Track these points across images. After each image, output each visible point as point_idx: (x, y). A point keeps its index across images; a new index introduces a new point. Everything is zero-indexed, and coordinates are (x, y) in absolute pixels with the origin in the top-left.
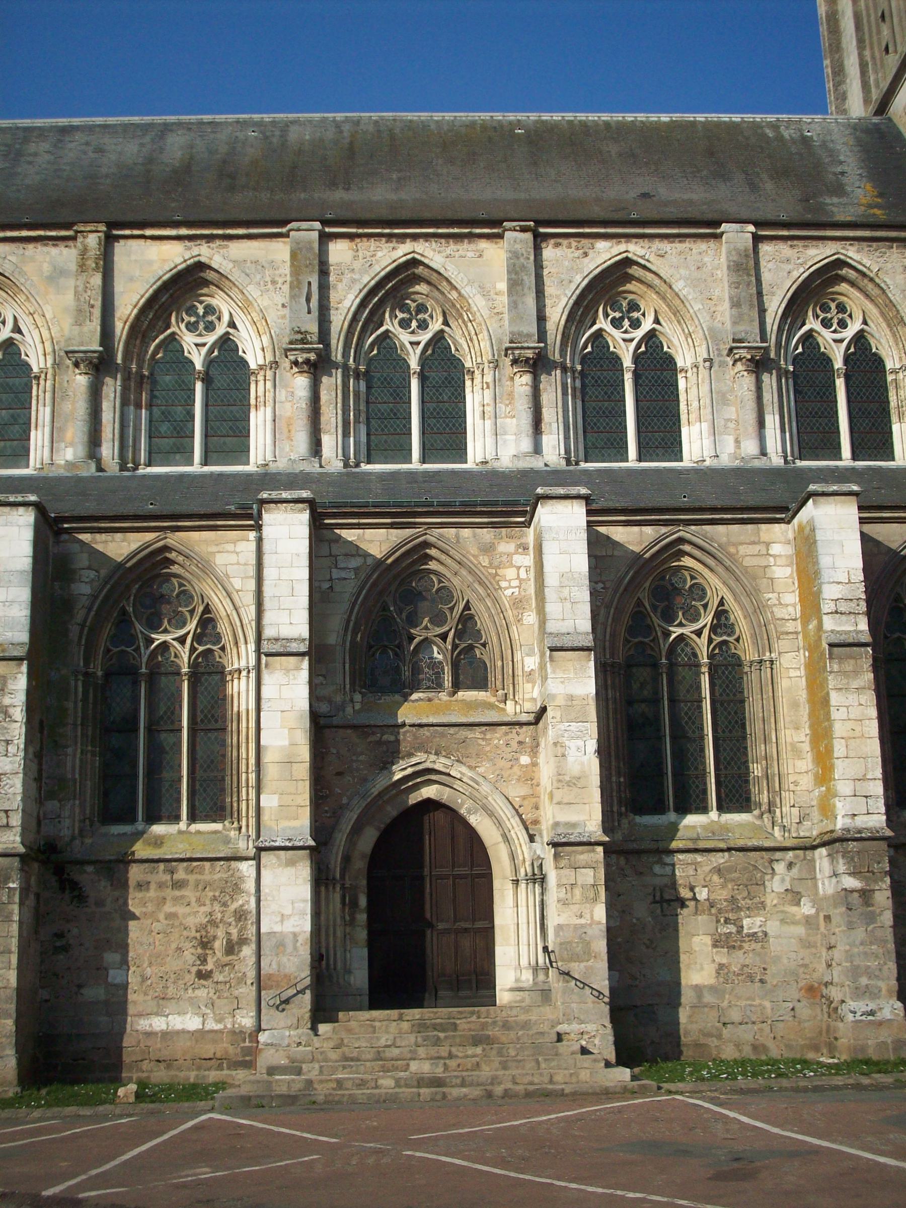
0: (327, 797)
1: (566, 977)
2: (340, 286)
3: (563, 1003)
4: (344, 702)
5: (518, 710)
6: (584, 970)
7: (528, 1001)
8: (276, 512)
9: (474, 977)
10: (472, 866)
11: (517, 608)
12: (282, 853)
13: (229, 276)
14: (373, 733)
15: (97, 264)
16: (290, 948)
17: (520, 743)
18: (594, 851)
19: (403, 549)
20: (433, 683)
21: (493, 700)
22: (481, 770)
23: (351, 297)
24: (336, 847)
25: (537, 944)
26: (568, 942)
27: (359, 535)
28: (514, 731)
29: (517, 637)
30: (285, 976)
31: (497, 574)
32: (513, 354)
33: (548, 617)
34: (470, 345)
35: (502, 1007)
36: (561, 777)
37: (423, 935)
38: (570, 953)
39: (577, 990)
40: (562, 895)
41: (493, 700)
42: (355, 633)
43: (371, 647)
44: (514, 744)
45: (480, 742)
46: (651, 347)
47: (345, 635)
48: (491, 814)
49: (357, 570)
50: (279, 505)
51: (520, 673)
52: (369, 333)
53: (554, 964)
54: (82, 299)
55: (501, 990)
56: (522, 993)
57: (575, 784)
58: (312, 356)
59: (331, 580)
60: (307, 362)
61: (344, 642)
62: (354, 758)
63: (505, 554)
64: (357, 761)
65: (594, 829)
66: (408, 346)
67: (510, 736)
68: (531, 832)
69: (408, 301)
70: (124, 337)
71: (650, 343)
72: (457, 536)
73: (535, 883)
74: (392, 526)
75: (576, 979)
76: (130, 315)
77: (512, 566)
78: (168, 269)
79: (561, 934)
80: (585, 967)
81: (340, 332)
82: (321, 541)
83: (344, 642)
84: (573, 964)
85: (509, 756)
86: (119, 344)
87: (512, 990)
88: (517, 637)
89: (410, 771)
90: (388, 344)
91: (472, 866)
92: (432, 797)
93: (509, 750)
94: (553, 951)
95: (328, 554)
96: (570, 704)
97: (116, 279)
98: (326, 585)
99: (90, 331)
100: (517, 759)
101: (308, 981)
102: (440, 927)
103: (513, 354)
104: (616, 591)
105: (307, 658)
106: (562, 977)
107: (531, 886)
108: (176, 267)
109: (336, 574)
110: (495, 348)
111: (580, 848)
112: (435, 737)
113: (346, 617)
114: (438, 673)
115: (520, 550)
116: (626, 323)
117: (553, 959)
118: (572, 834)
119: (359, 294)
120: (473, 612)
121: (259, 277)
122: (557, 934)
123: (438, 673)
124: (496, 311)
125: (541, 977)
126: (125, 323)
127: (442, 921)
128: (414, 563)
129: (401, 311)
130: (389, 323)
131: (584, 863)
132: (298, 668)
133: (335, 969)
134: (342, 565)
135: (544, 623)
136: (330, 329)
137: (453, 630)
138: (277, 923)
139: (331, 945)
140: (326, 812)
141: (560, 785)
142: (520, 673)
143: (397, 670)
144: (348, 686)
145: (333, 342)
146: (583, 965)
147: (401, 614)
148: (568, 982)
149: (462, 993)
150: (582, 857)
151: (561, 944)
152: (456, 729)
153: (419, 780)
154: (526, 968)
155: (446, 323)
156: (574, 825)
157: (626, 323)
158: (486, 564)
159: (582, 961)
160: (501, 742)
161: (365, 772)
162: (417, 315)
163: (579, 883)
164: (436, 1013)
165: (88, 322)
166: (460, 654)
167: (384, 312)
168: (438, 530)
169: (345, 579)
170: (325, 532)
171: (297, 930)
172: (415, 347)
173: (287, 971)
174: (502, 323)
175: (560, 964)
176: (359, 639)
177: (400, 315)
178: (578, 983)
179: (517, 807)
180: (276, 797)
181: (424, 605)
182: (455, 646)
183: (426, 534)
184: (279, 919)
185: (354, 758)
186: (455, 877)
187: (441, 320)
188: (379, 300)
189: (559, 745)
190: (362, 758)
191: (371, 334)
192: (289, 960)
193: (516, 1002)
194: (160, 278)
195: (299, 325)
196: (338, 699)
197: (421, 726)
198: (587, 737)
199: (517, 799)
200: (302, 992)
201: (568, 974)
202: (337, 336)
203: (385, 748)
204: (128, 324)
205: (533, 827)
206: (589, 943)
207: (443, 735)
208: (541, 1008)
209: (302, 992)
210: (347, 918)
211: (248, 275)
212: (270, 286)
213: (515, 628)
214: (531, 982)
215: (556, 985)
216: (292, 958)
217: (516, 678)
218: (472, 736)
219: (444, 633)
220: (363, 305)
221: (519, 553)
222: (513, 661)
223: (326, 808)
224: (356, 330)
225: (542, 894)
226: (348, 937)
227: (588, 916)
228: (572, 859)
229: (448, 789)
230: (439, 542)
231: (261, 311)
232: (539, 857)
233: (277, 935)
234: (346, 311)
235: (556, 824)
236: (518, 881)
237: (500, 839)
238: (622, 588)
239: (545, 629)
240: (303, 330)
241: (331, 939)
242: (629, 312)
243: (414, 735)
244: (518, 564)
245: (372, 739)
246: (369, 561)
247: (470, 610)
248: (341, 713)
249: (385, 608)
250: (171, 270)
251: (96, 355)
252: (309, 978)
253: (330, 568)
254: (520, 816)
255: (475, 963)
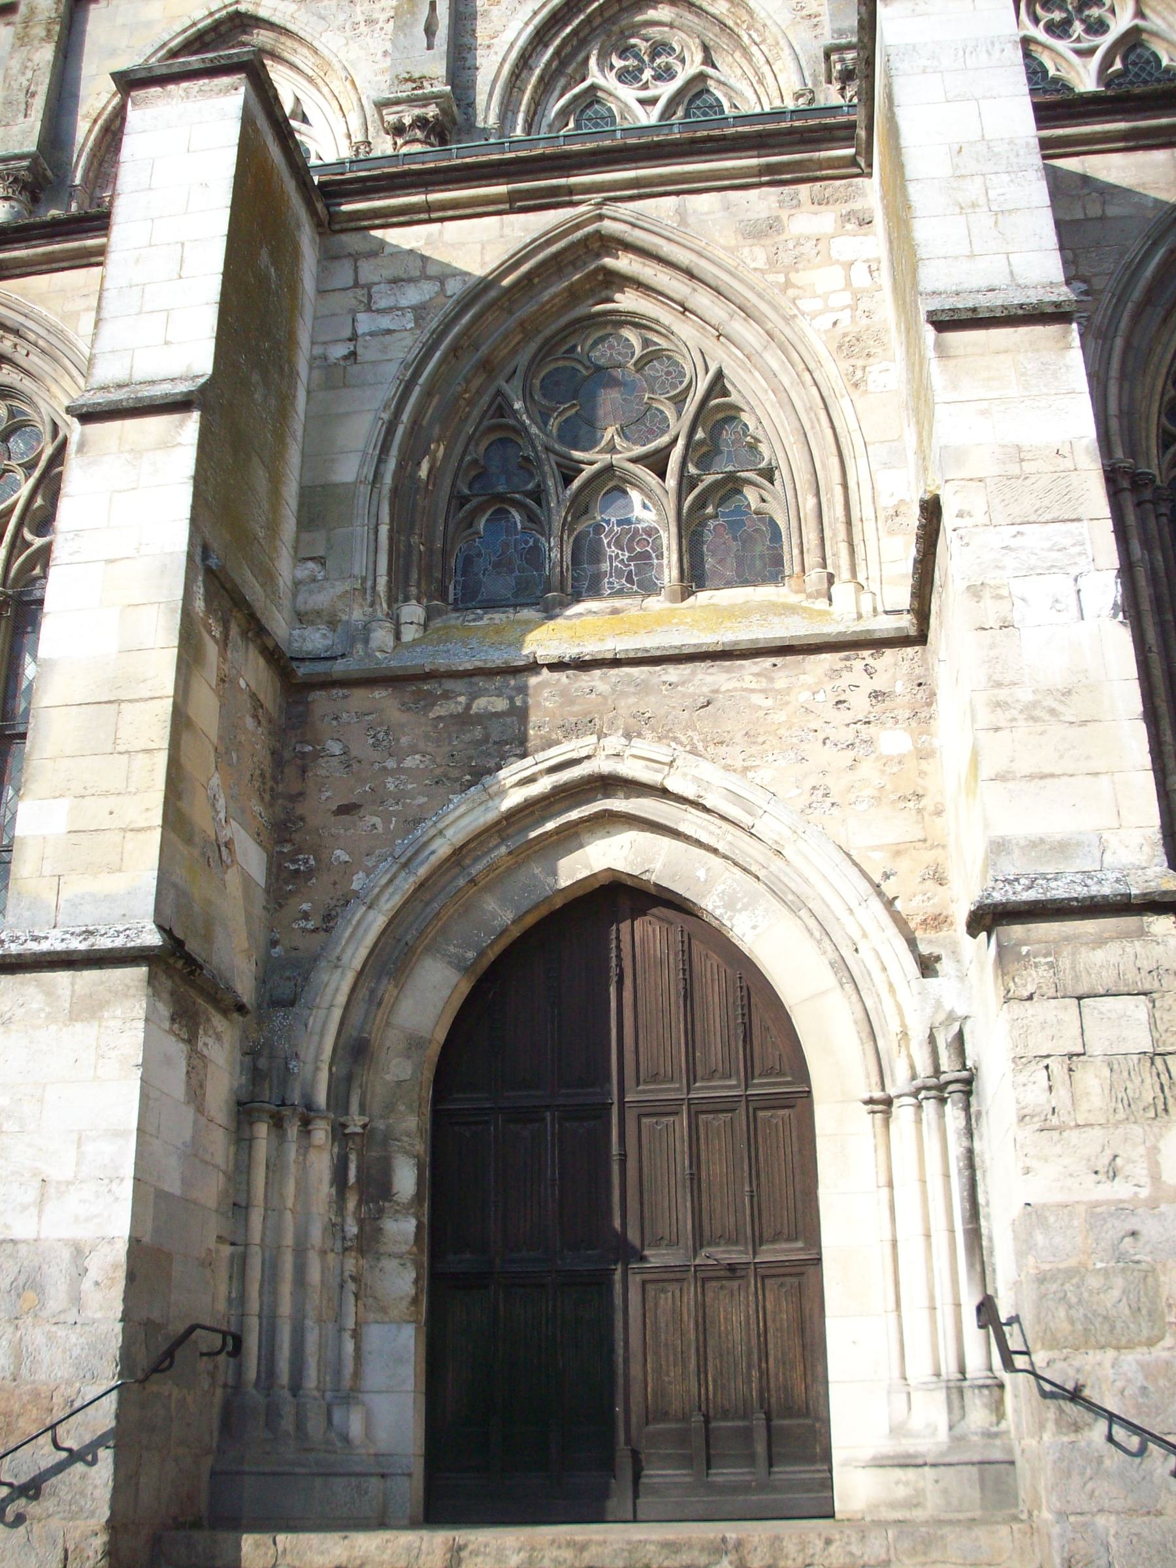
0: (310, 873)
1: (1068, 1407)
2: (495, 11)
3: (1062, 1515)
4: (373, 618)
5: (866, 609)
6: (1140, 1380)
7: (932, 1505)
8: (160, 102)
9: (758, 1421)
10: (749, 1076)
11: (848, 357)
12: (62, 978)
13: (290, 26)
14: (447, 696)
15: (49, 31)
16: (57, 1297)
17: (876, 695)
18: (1142, 933)
19: (541, 256)
20: (630, 580)
21: (794, 599)
22: (764, 775)
23: (516, 24)
24: (322, 1013)
25: (958, 1305)
26: (1070, 1273)
27: (429, 236)
28: (858, 665)
29: (853, 426)
30: (36, 1395)
31: (788, 284)
32: (842, 60)
33: (922, 252)
34: (760, 90)
35: (862, 1527)
36: (1002, 694)
37: (600, 1283)
38: (1078, 1313)
39: (1114, 1460)
40: (1036, 1096)
41: (794, 599)
42: (411, 459)
43: (463, 500)
44: (860, 703)
45: (757, 699)
46: (1134, 64)
47: (381, 460)
48: (795, 904)
49: (420, 312)
50: (171, 87)
51: (868, 513)
52: (557, 93)
53: (1020, 1361)
54: (15, 86)
55: (845, 1464)
56: (911, 1474)
57: (1052, 712)
58: (432, 111)
59: (354, 338)
60: (421, 122)
61: (378, 476)
62: (391, 764)
63: (808, 238)
64: (400, 770)
65: (1141, 858)
66: (637, 107)
67: (847, 679)
68: (924, 949)
69: (633, 41)
70: (90, 144)
71: (1132, 57)
72: (682, 215)
73: (942, 1101)
74: (515, 204)
75: (1112, 1418)
76: (104, 108)
77: (830, 261)
78: (179, 30)
79: (1040, 1238)
80: (1143, 1366)
81: (495, 81)
82: (336, 258)
83: (378, 476)
84: (1094, 1357)
85: (848, 735)
86: (79, 156)
87: (880, 1463)
88: (853, 426)
89: (544, 785)
90: (596, 112)
91: (749, 1076)
92: (621, 865)
93: (848, 716)
94: (1014, 1320)
95: (351, 283)
96: (1014, 469)
97: (86, 58)
98: (340, 351)
99: (23, 132)
100: (869, 742)
101: (104, 1416)
102: (654, 1262)
103: (842, 60)
104: (1121, 299)
105: (196, 415)
106: (1051, 1410)
107: (930, 1106)
108: (194, 24)
109: (365, 324)
110: (806, 74)
111: (1089, 926)
112: (623, 694)
113: (386, 416)
114: (646, 556)
115: (849, 226)
116: (1078, 28)
117: (1014, 1344)
118: (1057, 876)
119: (531, 19)
120: (734, 398)
121: (342, 17)
122: (1024, 1247)
123: (646, 556)
124: (805, 13)
125: (978, 1416)
126: (95, 121)
127: (657, 1243)
128: (574, 296)
129: (621, 56)
130: (598, 74)
131: (1107, 980)
132: (166, 445)
133: (296, 1387)
134: (382, 304)
135: (914, 271)
136: (474, 82)
137: (681, 442)
138: (24, 1208)
139: (285, 1307)
140: (306, 916)
141: (1001, 718)
142: (868, 513)
143: (535, 556)
144: (382, 581)
145: (481, 99)
146: (1130, 1359)
147: (546, 423)
148: (1077, 1428)
149: (723, 1475)
150: (1099, 956)
151: (1042, 1279)
152: (685, 669)
153: (574, 815)
154: (925, 1387)
155: (708, 61)
156: (1063, 848)
157: (1078, 28)
158: (761, 263)
159: (1130, 1346)
160: (820, 697)
161: (422, 800)
162: (652, 60)
163: (1096, 1048)
164: (583, 1547)
165: (21, 118)
166: (700, 503)
167: (587, 59)
168: (631, 205)
169: (389, 332)
170: (345, 238)
171: (83, 1233)
172: (649, 108)
173: (42, 1376)
174: (818, 31)
175: (1040, 1358)
176: (423, 473)
177: (618, 63)
178: (1119, 1433)
179: (877, 879)
180: (65, 804)
181: (609, 399)
182: (686, 483)
183: (601, 217)
184: (31, 1195)
185: (391, 764)
186: (697, 1110)
187: (699, 56)
188: (572, 31)
189: (987, 594)
190: (411, 762)
191: (562, 95)
192: (50, 1338)
193: (893, 1505)
194: (165, 44)
195: (408, 69)
196: (357, 615)
197: (582, 665)
198: (1083, 564)
199: (877, 855)
200: (84, 1455)
201: (1075, 1396)
202: (488, 89)
203: (478, 732)
204: (100, 122)
205: (931, 934)
206: (1150, 1272)
207: (643, 688)
208: (980, 1532)
209: (84, 1455)
210: (352, 1229)
211: (324, 19)
212: (363, 28)
213: (845, 403)
214: (943, 1435)
215: (1031, 1442)
216: (61, 1332)
217: (856, 530)
218: (733, 684)
219: (657, 451)
220: (541, 37)
221: (848, 234)
222: (845, 486)
223: (305, 907)
224: (528, 82)
225: (970, 1133)
226: (351, 1286)
227: (1140, 1171)
228: (1065, 963)
229: (665, 842)
230: (638, 233)
231: (345, 68)
232: (951, 1017)
233: (23, 1249)
234: (506, 47)
235: (999, 847)
236: (888, 1102)
237: (829, 979)
238: (1137, 294)
239: (915, 283)
240: (416, 75)
241: (286, 1289)
242: (1080, 9)
243: (564, 693)
244: (847, 257)
245: (439, 711)
246: (454, 287)
247: (725, 393)
248: (359, 646)
249: (501, 407)
250: (184, 31)
251: (25, 163)
252: (110, 1404)
253: (353, 312)
254: (889, 904)
255: (764, 1374)
